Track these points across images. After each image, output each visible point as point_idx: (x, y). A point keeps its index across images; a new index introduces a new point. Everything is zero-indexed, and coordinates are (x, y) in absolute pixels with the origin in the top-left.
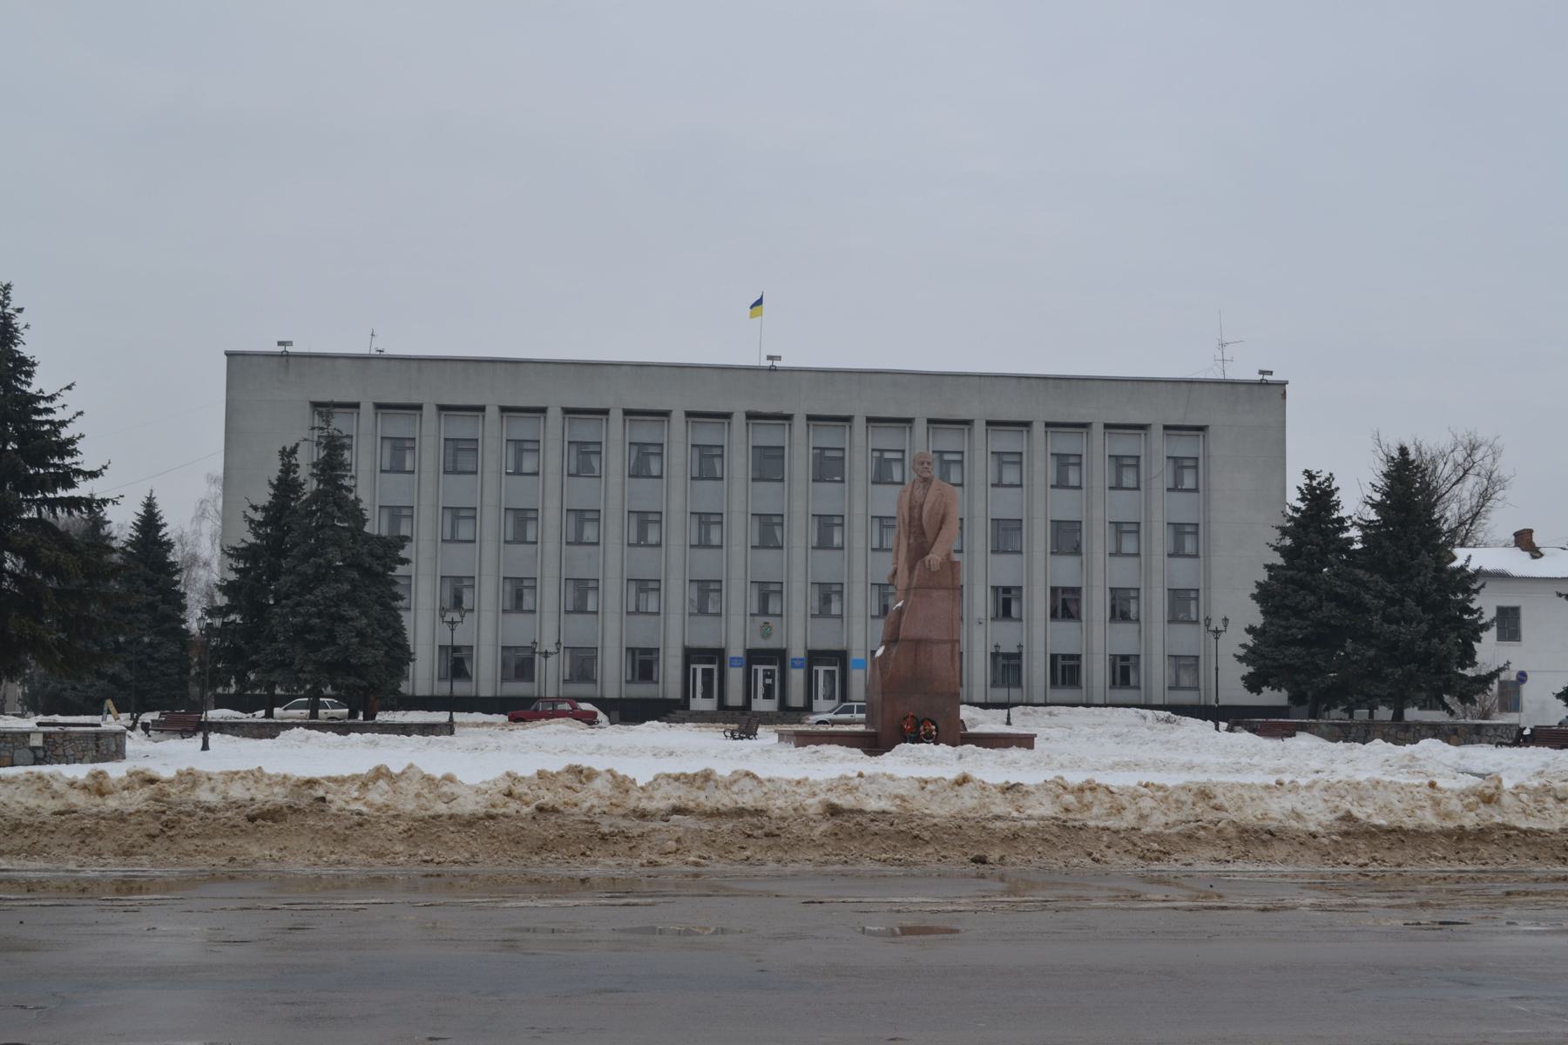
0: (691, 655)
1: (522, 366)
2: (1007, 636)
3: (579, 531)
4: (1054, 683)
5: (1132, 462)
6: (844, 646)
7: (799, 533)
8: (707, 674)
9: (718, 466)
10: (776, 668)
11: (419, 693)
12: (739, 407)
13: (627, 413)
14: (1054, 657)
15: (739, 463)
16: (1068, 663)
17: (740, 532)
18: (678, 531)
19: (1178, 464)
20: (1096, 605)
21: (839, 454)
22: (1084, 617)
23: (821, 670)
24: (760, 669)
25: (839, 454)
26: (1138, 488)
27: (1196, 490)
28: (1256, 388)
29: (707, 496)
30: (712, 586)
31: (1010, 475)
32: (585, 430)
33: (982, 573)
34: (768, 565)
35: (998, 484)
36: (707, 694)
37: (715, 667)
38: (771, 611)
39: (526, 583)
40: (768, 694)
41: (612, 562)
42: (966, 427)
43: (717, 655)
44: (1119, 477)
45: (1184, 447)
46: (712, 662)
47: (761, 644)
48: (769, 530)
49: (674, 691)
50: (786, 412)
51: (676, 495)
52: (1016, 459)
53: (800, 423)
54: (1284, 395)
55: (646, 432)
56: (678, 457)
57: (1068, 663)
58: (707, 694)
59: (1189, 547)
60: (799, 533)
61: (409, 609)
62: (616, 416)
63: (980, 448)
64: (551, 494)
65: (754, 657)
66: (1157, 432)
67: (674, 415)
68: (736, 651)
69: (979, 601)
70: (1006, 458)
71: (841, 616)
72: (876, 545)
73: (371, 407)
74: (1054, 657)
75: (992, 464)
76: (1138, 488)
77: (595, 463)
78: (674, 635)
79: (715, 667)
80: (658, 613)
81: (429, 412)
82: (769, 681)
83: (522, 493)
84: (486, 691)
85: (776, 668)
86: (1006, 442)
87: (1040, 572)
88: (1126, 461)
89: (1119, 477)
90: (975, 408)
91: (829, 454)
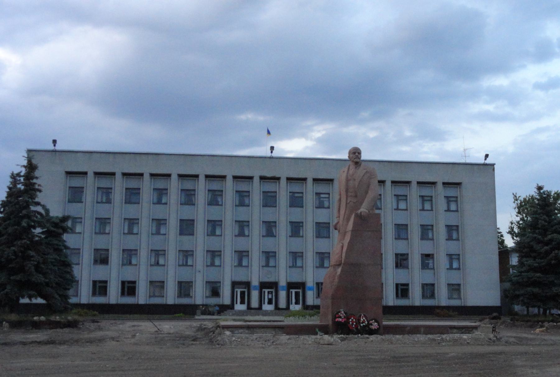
0: (235, 284)
1: (160, 156)
2: (402, 276)
4: (123, 294)
5: (429, 198)
7: (283, 230)
8: (297, 294)
9: (193, 199)
10: (273, 290)
11: (442, 305)
12: (310, 176)
13: (207, 176)
14: (397, 285)
15: (256, 198)
16: (403, 287)
17: (256, 229)
18: (229, 229)
19: (448, 199)
20: (415, 261)
21: (301, 195)
22: (410, 267)
23: (293, 291)
24: (266, 291)
26: (432, 210)
27: (457, 211)
28: (482, 167)
29: (269, 214)
30: (244, 254)
31: (402, 205)
32: (188, 185)
33: (390, 247)
34: (269, 244)
35: (397, 209)
36: (242, 302)
37: (300, 291)
38: (270, 265)
39: (271, 254)
40: (270, 302)
41: (228, 242)
42: (331, 182)
43: (247, 285)
44: (448, 206)
45: (451, 192)
46: (271, 288)
47: (266, 280)
48: (270, 228)
49: (227, 301)
50: (278, 176)
51: (256, 213)
52: (405, 198)
53: (283, 182)
54: (494, 169)
55: (133, 183)
56: (229, 197)
57: (403, 287)
58: (242, 302)
59: (455, 236)
60: (283, 230)
61: (78, 264)
62: (202, 178)
63: (389, 191)
64: (201, 212)
65: (263, 285)
66: (440, 186)
67: (228, 178)
68: (255, 283)
69: (389, 261)
70: (426, 198)
71: (302, 267)
73: (231, 178)
74: (397, 285)
75: (394, 200)
76: (432, 210)
77: (219, 200)
78: (227, 275)
79: (300, 291)
80: (220, 266)
81: (118, 176)
82: (270, 296)
83: (159, 212)
84: (142, 301)
85: (273, 290)
86: (401, 190)
87: (416, 247)
88: (426, 198)
89: (448, 206)
90: (413, 177)
91: (296, 195)
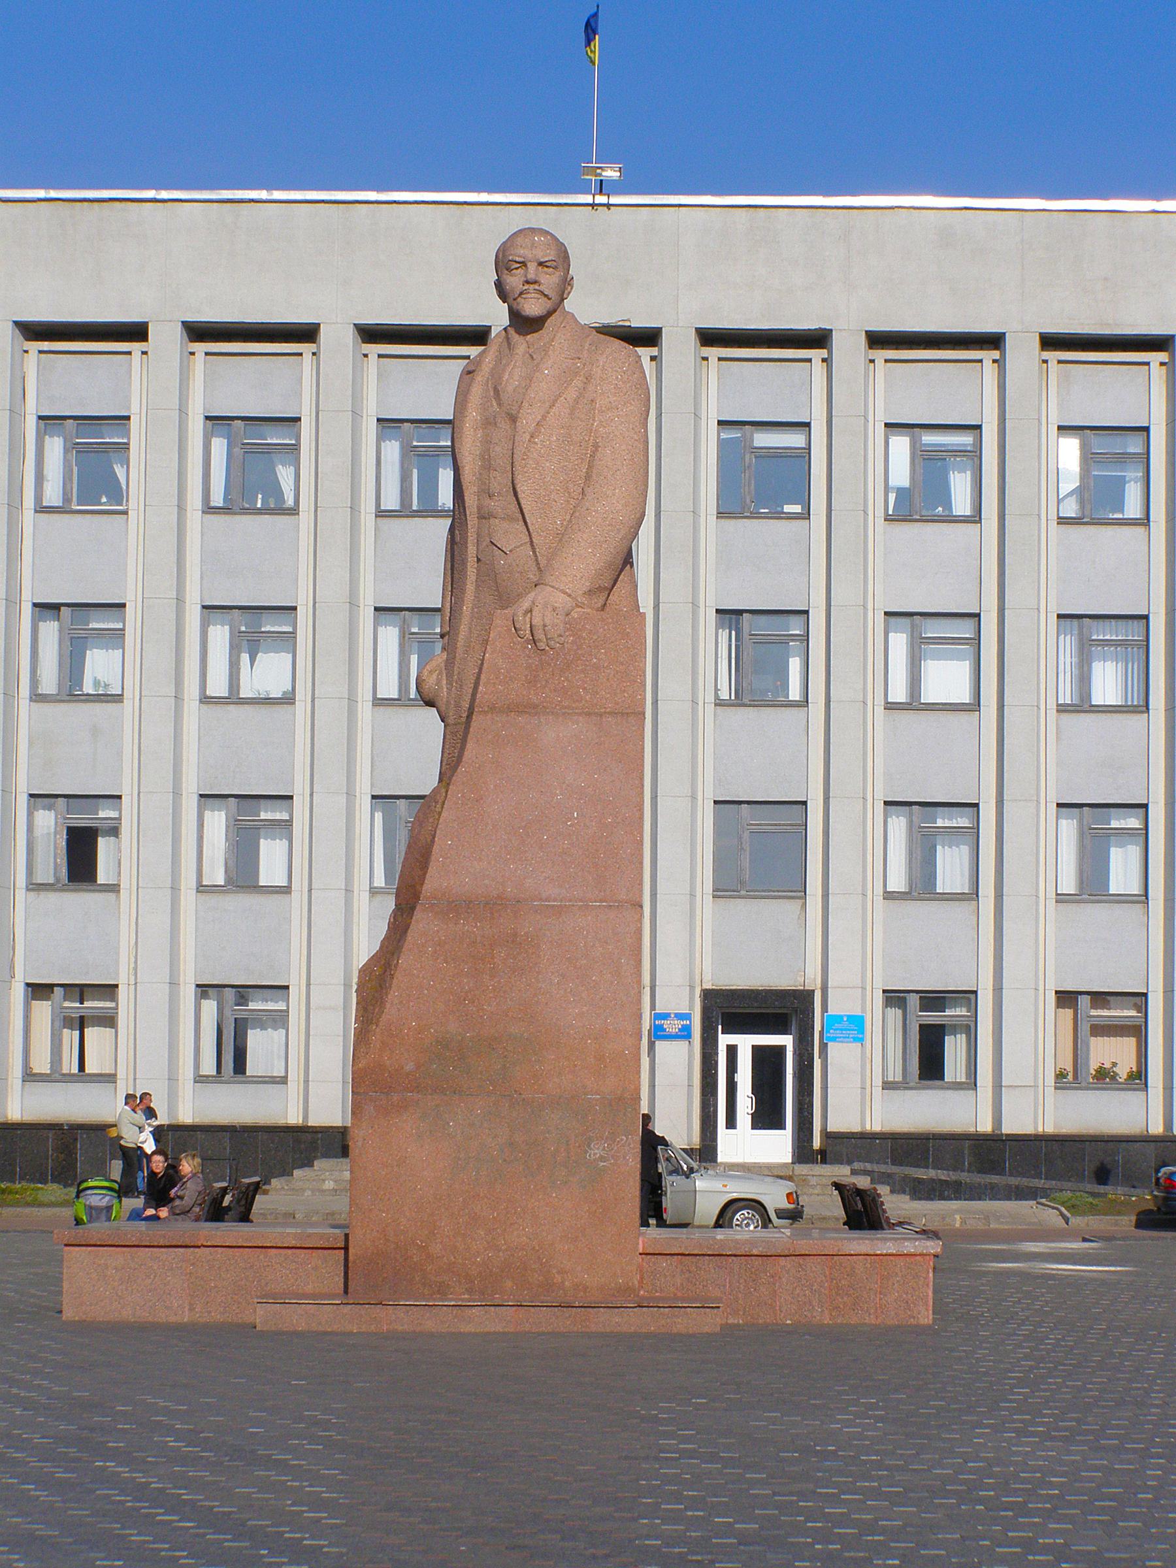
3: (72, 667)
6: (811, 979)
8: (768, 1063)
21: (795, 440)
25: (795, 440)
36: (767, 1115)
46: (778, 1024)
50: (639, 322)
72: (899, 694)
91: (764, 439)
